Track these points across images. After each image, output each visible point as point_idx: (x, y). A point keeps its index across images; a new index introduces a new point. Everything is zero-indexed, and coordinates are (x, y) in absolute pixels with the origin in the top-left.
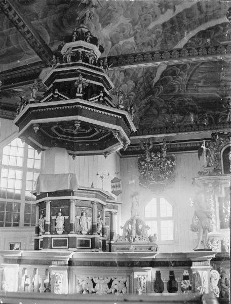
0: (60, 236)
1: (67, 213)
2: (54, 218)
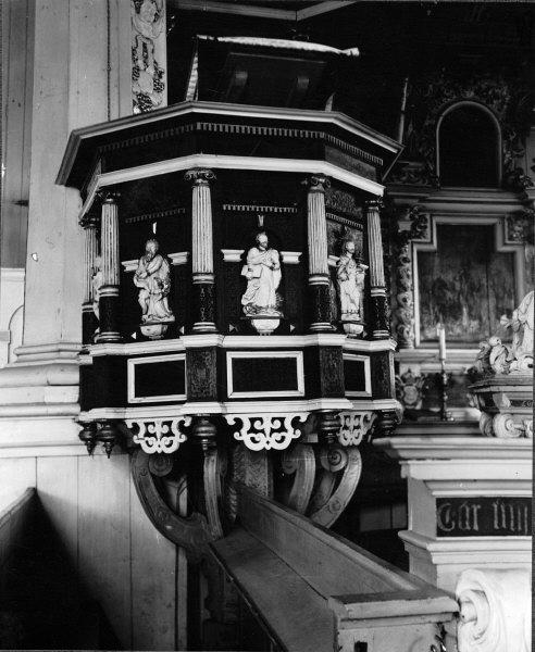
0: (266, 340)
1: (291, 235)
2: (232, 255)
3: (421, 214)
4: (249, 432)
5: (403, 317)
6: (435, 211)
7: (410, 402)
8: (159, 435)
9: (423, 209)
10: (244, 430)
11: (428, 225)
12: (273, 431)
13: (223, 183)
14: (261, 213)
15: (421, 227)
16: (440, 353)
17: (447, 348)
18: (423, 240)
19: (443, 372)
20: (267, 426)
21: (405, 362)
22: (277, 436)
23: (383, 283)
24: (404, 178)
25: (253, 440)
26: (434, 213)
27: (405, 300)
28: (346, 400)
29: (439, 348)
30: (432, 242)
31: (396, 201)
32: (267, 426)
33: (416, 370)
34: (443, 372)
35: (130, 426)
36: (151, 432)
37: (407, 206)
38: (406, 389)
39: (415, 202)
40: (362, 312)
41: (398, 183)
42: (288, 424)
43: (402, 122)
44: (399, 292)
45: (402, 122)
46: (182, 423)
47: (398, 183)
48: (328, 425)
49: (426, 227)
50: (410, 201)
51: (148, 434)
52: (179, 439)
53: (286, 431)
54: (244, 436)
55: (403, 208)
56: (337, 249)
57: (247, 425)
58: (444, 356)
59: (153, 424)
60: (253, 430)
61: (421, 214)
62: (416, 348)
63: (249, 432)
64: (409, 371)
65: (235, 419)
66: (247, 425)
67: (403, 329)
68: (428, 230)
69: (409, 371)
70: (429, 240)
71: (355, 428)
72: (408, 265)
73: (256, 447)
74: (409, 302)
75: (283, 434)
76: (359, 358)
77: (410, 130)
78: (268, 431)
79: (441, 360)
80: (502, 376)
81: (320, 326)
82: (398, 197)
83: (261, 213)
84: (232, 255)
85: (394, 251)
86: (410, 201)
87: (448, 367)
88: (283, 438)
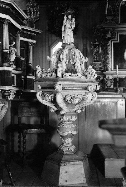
3: (114, 32)
5: (107, 62)
6: (118, 31)
7: (109, 86)
9: (114, 31)
11: (116, 35)
15: (114, 36)
16: (117, 72)
17: (119, 71)
18: (115, 40)
19: (117, 77)
21: (107, 75)
24: (108, 22)
26: (118, 32)
27: (108, 57)
28: (12, 87)
29: (116, 71)
30: (117, 40)
31: (106, 28)
33: (111, 77)
34: (117, 77)
37: (109, 30)
38: (107, 82)
39: (112, 28)
40: (15, 62)
41: (106, 23)
43: (107, 4)
44: (107, 55)
45: (107, 4)
47: (106, 23)
48: (6, 94)
49: (115, 36)
50: (109, 28)
55: (108, 31)
56: (10, 43)
58: (118, 73)
61: (114, 32)
62: (111, 70)
64: (109, 77)
67: (107, 65)
68: (116, 37)
69: (109, 77)
70: (116, 40)
71: (12, 95)
72: (109, 47)
74: (109, 58)
76: (114, 70)
77: (110, 7)
79: (117, 74)
81: (7, 64)
82: (106, 27)
85: (106, 43)
86: (109, 28)
87: (119, 76)
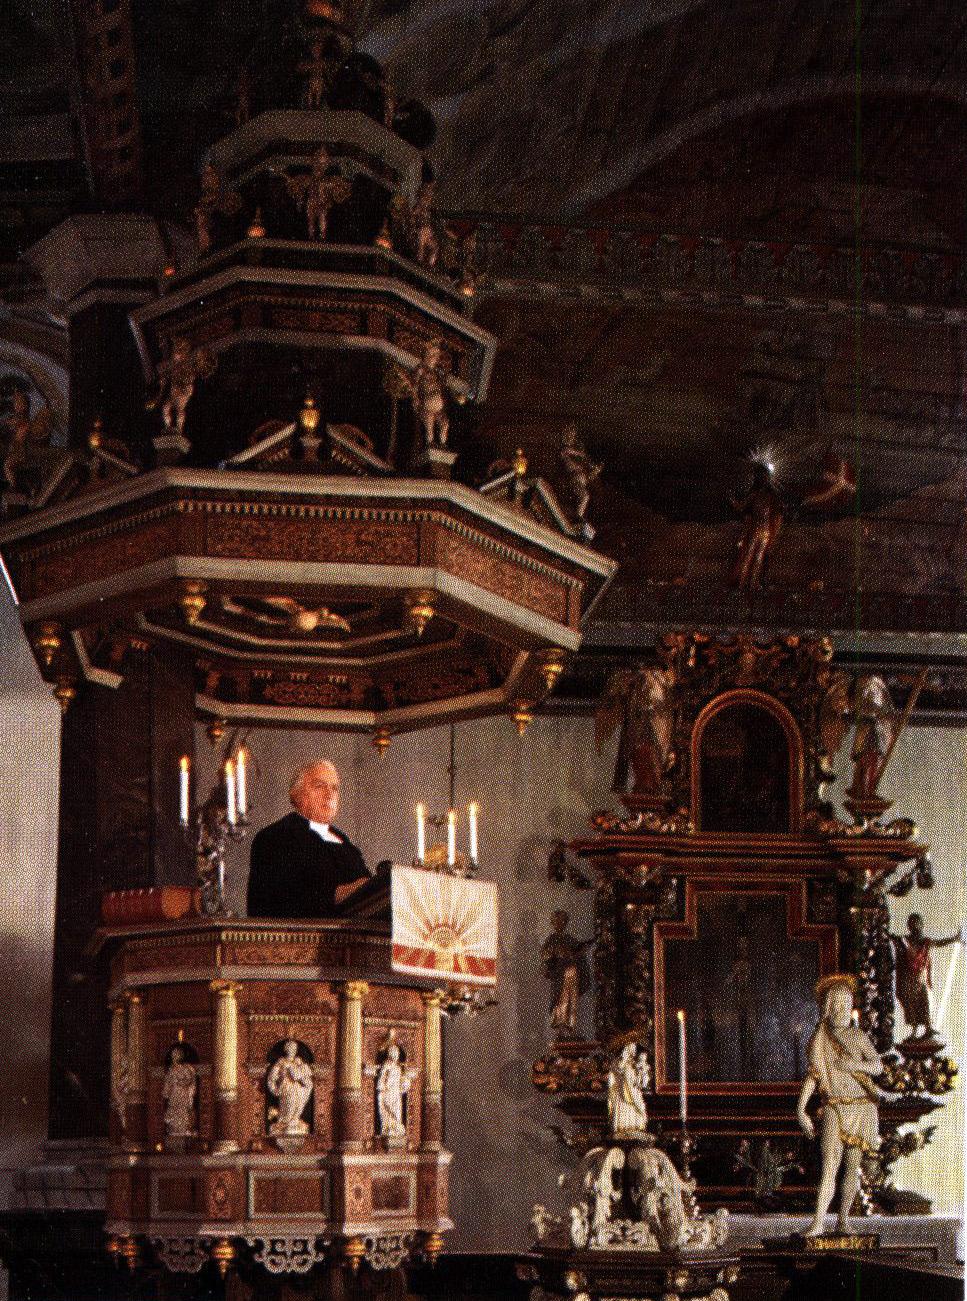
4: (269, 1254)
8: (289, 1254)
10: (264, 1252)
12: (294, 1253)
13: (771, 1139)
14: (744, 1137)
20: (288, 1250)
22: (298, 1259)
23: (430, 571)
25: (273, 1262)
32: (288, 1250)
35: (251, 1244)
36: (279, 1250)
42: (310, 1247)
43: (726, 1133)
46: (408, 1237)
51: (273, 1252)
52: (314, 1258)
53: (308, 1253)
54: (265, 1259)
57: (267, 1248)
59: (283, 1242)
60: (273, 1252)
63: (269, 1254)
65: (256, 1241)
66: (267, 1248)
73: (275, 1270)
75: (305, 1257)
78: (289, 1254)
80: (821, 1245)
83: (744, 1137)
84: (921, 1030)
88: (305, 1262)
